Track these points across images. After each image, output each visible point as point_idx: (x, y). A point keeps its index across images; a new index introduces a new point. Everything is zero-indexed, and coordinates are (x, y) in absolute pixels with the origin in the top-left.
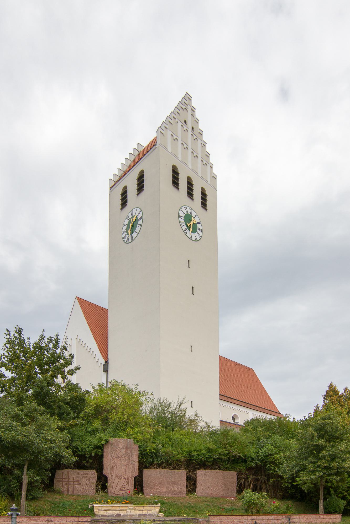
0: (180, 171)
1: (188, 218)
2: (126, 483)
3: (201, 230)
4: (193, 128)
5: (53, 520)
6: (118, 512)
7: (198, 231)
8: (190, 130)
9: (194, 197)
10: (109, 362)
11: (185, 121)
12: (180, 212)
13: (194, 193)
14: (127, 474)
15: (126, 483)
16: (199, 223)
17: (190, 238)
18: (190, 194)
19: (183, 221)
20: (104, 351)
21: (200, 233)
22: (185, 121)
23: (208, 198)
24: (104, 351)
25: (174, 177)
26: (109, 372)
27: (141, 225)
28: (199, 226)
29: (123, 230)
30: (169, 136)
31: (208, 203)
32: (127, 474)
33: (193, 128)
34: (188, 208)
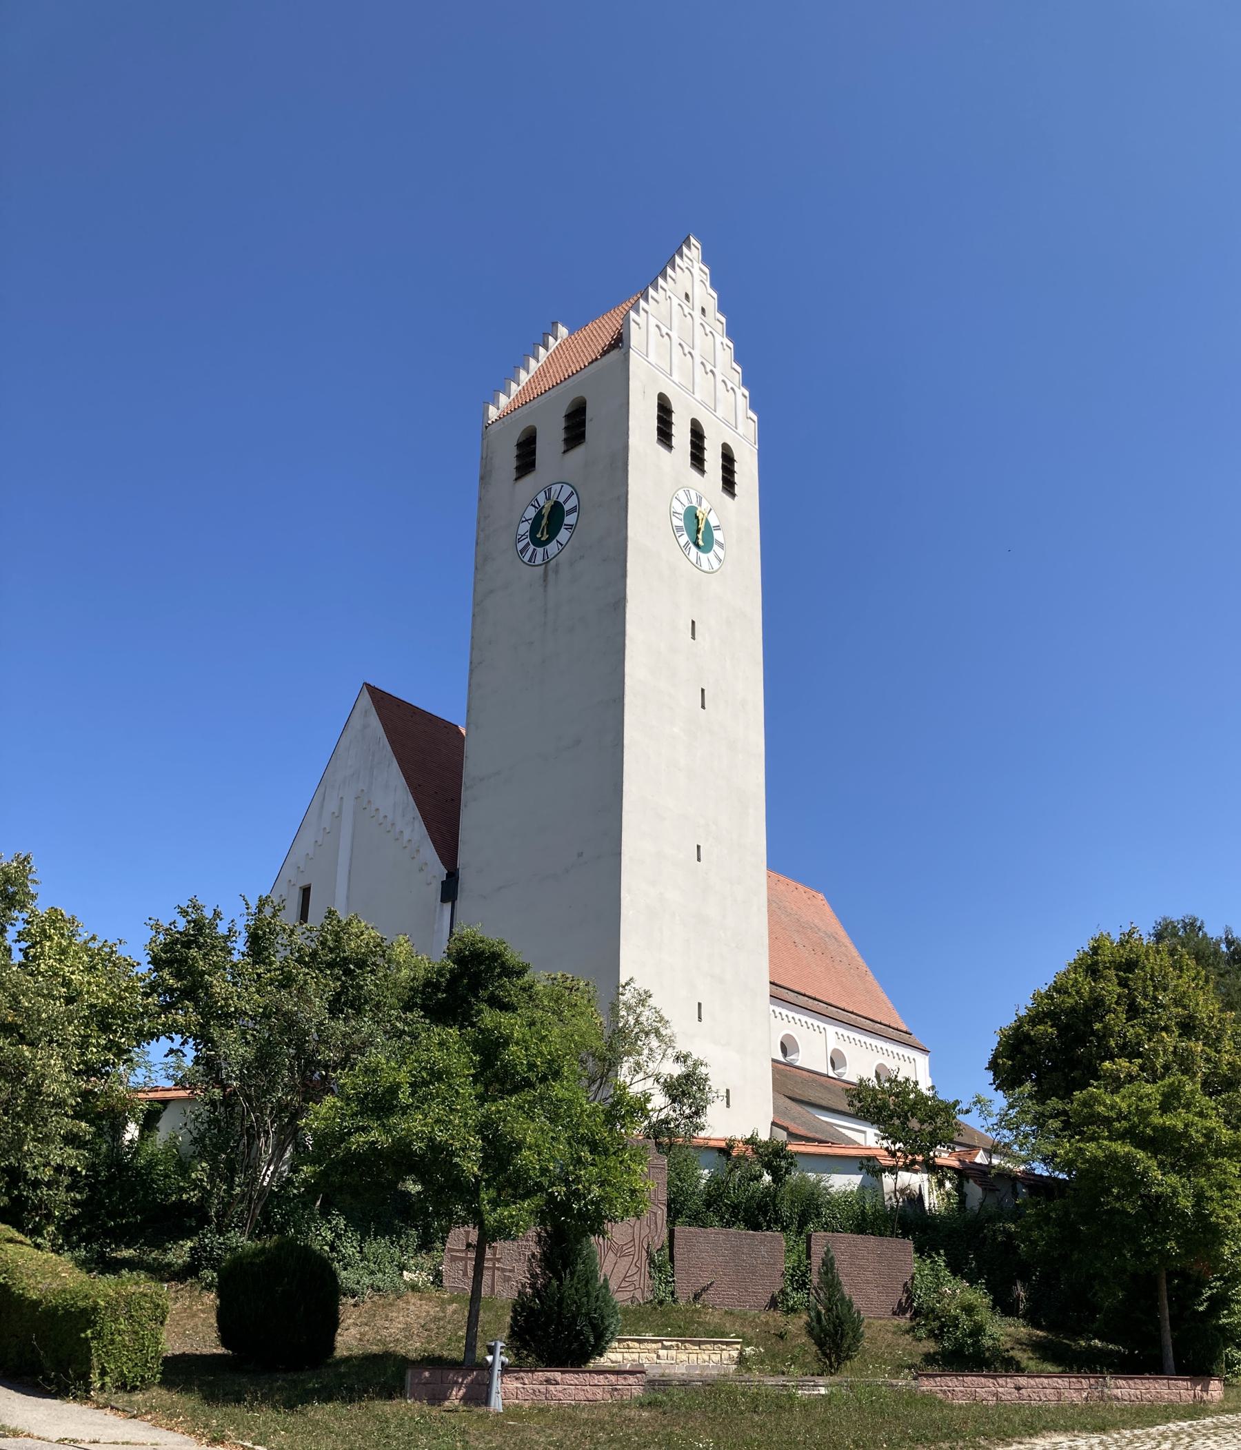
0: (675, 407)
1: (692, 517)
2: (635, 1270)
3: (721, 545)
4: (703, 310)
5: (559, 1379)
6: (635, 1356)
7: (715, 547)
8: (697, 313)
9: (674, 441)
10: (463, 875)
11: (687, 296)
12: (676, 504)
13: (707, 455)
14: (637, 1242)
15: (635, 1270)
16: (718, 528)
17: (697, 565)
18: (698, 460)
19: (681, 524)
20: (446, 840)
21: (721, 553)
22: (687, 296)
23: (737, 467)
24: (446, 840)
25: (660, 419)
26: (458, 903)
27: (570, 527)
28: (718, 535)
29: (521, 532)
30: (653, 329)
31: (737, 478)
32: (637, 1242)
33: (703, 310)
34: (693, 493)
